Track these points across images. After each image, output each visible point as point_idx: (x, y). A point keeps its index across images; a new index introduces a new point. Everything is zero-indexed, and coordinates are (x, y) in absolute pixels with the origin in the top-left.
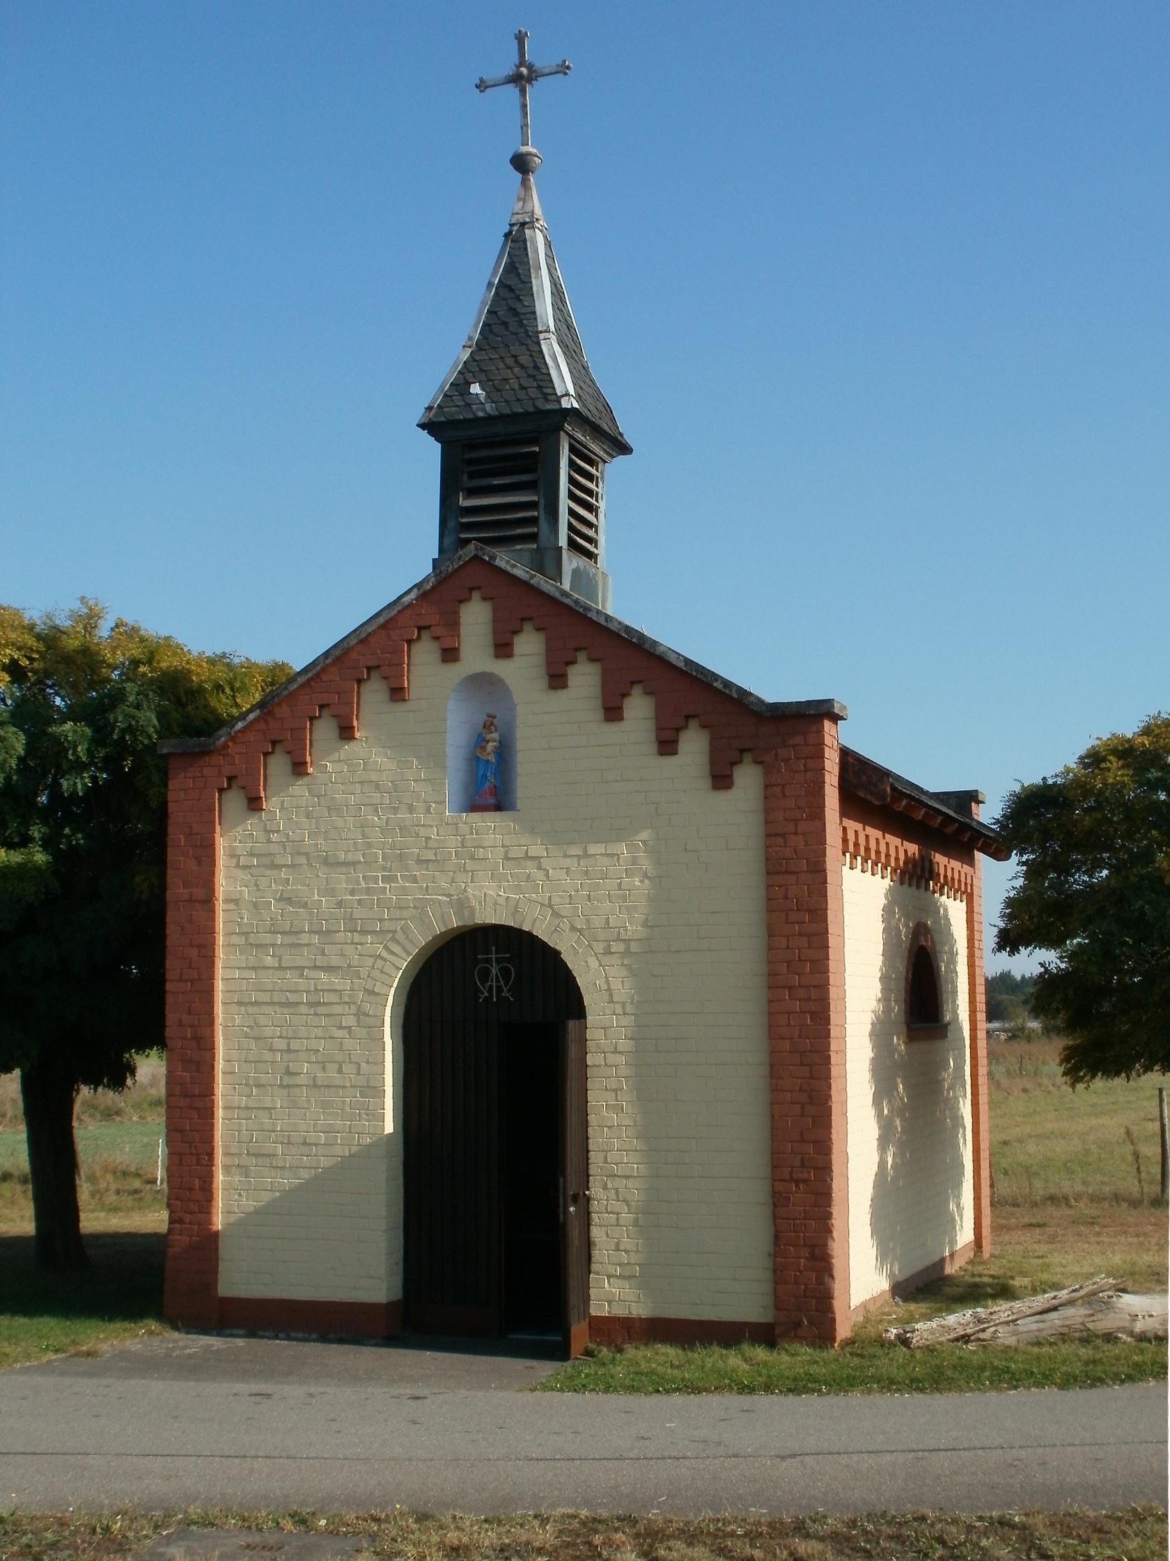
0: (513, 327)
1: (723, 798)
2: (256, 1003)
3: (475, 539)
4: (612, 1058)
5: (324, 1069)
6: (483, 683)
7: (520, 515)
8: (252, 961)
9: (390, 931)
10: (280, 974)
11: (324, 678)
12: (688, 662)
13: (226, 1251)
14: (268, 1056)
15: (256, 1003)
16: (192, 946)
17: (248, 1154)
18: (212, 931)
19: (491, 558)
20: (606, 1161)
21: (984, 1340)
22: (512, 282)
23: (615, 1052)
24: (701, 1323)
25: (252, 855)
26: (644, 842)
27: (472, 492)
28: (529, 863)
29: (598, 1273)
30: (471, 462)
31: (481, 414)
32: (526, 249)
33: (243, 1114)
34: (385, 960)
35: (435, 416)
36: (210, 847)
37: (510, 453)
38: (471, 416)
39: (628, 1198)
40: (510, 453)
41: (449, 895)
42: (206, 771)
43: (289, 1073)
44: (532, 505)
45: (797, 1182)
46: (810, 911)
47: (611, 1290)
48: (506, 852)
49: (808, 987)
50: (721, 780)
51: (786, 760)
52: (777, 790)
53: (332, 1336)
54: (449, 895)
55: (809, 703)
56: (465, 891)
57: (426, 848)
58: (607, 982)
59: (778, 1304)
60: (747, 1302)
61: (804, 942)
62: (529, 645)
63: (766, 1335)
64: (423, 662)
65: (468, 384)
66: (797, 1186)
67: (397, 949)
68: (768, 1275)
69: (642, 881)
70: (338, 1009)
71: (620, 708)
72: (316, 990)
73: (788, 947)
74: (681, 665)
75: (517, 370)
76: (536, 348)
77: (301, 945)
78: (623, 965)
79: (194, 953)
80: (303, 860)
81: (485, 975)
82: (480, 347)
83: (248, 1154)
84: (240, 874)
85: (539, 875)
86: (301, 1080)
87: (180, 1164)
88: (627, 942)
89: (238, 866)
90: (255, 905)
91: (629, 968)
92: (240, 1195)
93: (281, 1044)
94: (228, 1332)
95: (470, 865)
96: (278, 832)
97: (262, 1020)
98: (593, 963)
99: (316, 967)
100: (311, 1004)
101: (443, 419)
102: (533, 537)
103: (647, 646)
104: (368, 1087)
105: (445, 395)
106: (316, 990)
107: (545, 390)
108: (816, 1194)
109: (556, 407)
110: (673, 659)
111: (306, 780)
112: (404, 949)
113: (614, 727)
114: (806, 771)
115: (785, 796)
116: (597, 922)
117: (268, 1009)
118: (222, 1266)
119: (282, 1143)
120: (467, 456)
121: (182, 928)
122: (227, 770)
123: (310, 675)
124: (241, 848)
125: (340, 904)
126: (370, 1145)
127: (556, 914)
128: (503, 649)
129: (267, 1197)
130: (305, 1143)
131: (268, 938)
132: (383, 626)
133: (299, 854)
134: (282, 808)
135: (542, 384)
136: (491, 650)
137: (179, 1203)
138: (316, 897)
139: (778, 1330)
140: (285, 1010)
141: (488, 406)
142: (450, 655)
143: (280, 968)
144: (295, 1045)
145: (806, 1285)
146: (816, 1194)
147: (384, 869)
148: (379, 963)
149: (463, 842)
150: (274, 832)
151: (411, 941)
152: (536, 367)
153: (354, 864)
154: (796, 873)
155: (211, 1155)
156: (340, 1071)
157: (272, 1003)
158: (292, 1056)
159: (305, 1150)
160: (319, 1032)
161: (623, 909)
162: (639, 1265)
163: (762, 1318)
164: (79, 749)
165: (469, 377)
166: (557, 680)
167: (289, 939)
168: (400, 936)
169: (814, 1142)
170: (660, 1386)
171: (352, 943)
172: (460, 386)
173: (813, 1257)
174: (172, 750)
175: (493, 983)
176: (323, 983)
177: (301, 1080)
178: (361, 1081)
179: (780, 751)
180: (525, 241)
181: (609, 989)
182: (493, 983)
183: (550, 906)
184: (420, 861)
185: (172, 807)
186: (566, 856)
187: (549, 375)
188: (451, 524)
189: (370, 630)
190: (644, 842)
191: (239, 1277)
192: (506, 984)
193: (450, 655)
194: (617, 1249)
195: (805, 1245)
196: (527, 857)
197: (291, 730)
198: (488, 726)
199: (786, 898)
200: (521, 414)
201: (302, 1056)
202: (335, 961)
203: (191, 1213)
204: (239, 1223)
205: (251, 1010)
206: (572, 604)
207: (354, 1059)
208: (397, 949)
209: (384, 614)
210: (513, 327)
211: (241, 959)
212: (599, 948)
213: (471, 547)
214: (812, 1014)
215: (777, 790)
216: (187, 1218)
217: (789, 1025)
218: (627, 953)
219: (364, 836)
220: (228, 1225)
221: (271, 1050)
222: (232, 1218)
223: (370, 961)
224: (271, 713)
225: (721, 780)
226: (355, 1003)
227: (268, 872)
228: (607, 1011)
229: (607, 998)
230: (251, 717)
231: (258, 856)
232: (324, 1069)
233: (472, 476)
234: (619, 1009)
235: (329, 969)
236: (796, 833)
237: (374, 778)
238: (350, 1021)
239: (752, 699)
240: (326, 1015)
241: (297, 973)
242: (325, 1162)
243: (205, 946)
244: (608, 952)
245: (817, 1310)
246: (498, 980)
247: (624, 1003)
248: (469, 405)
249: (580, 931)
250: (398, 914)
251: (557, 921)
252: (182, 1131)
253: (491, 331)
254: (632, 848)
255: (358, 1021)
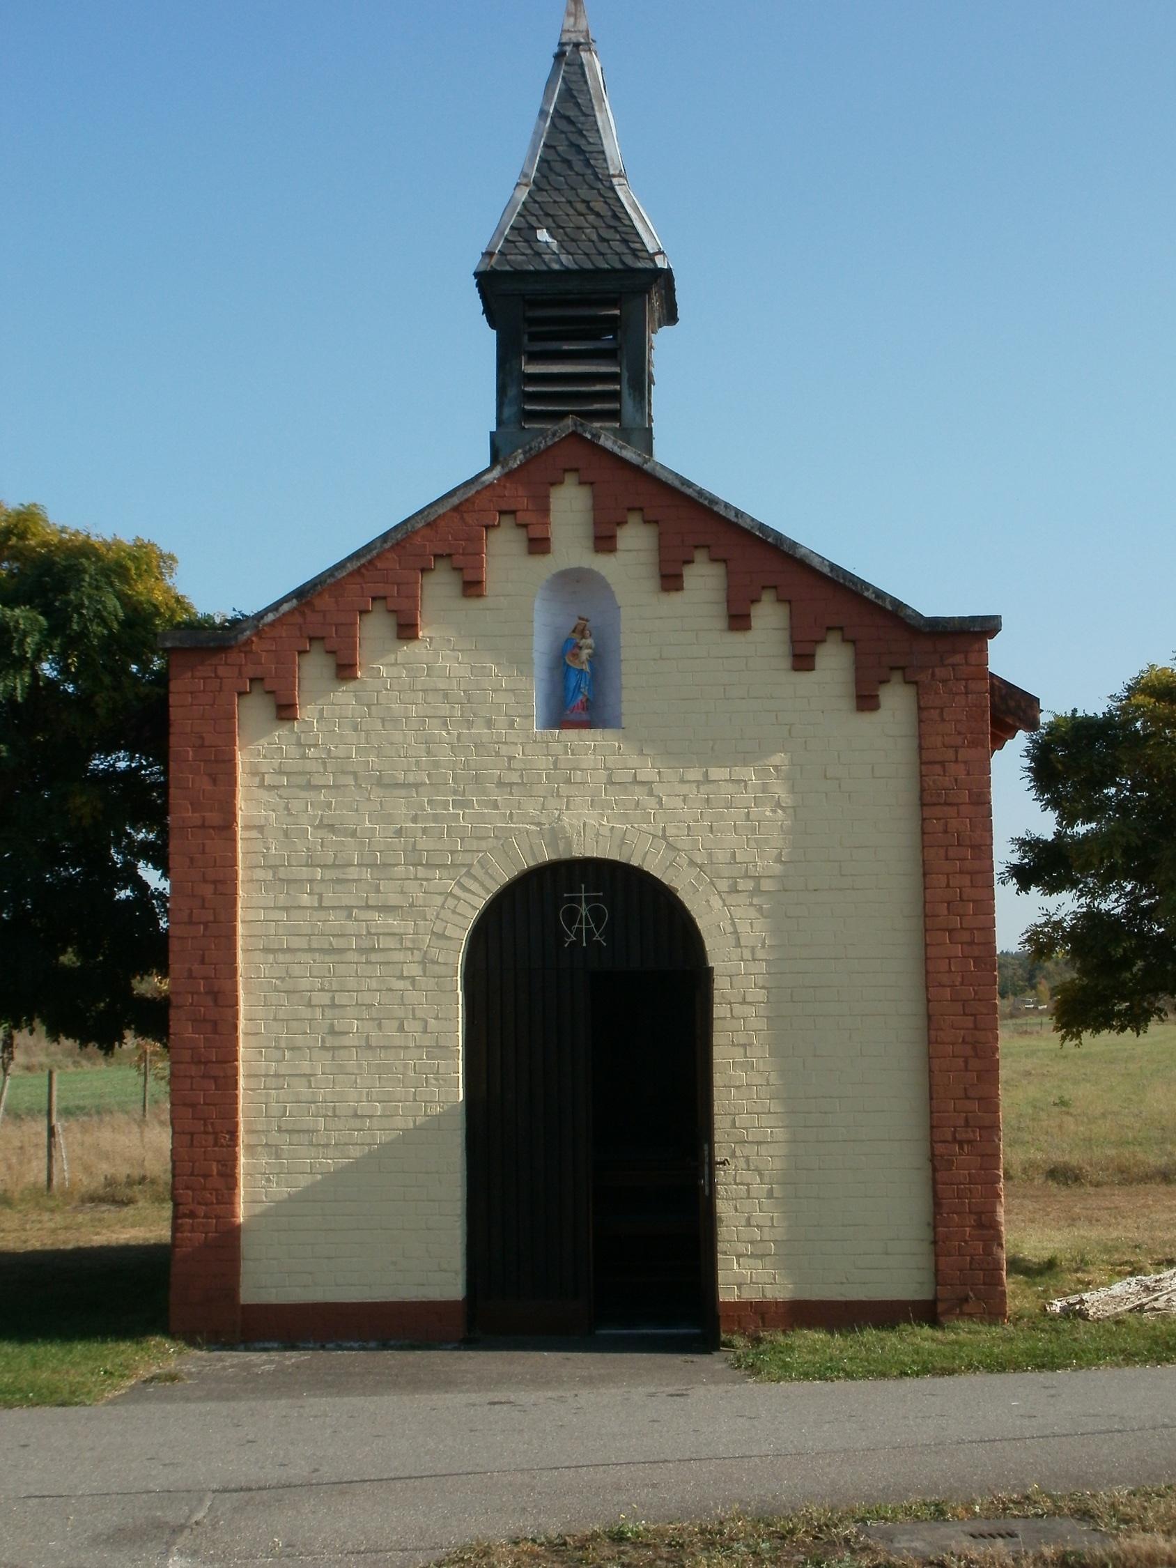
0: (578, 166)
1: (868, 720)
2: (289, 950)
3: (573, 412)
4: (738, 1010)
5: (380, 1027)
6: (573, 582)
7: (598, 388)
8: (282, 900)
9: (463, 865)
10: (322, 915)
11: (379, 565)
12: (833, 567)
13: (249, 1247)
14: (305, 1012)
15: (289, 950)
16: (205, 881)
17: (280, 1130)
18: (233, 863)
19: (593, 435)
20: (733, 1125)
21: (1159, 1310)
22: (572, 113)
23: (744, 1002)
24: (848, 1304)
25: (280, 772)
26: (776, 767)
27: (534, 357)
28: (637, 789)
29: (725, 1253)
30: (532, 321)
31: (556, 267)
32: (584, 75)
33: (272, 1082)
34: (459, 899)
35: (498, 263)
36: (232, 761)
37: (572, 315)
38: (544, 268)
39: (761, 1167)
40: (572, 315)
41: (539, 824)
42: (222, 671)
43: (333, 1032)
44: (614, 378)
45: (961, 1143)
46: (972, 847)
47: (746, 1269)
48: (610, 776)
49: (971, 929)
50: (866, 701)
51: (944, 681)
52: (935, 714)
53: (392, 1343)
54: (539, 824)
55: (973, 619)
56: (559, 819)
57: (509, 769)
58: (733, 924)
59: (938, 1276)
60: (899, 1274)
61: (966, 880)
62: (636, 540)
63: (928, 1313)
64: (502, 552)
65: (534, 229)
66: (961, 1148)
67: (474, 886)
68: (926, 1247)
69: (774, 811)
70: (398, 956)
71: (747, 617)
72: (369, 933)
73: (948, 886)
74: (826, 570)
75: (591, 218)
76: (610, 194)
77: (348, 880)
78: (751, 904)
79: (208, 890)
80: (350, 780)
81: (572, 915)
82: (538, 187)
83: (280, 1130)
84: (265, 795)
85: (652, 802)
86: (348, 1041)
87: (192, 1145)
88: (757, 879)
89: (261, 785)
90: (286, 834)
91: (760, 909)
92: (268, 1180)
93: (325, 999)
94: (257, 1345)
95: (564, 789)
96: (315, 746)
97: (296, 970)
98: (716, 902)
99: (368, 907)
100: (360, 950)
101: (508, 268)
102: (614, 415)
103: (785, 548)
104: (438, 1046)
105: (507, 240)
106: (369, 933)
107: (632, 245)
108: (982, 1156)
109: (649, 265)
110: (816, 563)
111: (352, 685)
112: (482, 885)
113: (738, 637)
114: (967, 693)
115: (943, 720)
116: (721, 856)
117: (306, 957)
118: (246, 1267)
119: (325, 1116)
120: (530, 314)
121: (192, 860)
122: (251, 670)
123: (363, 561)
124: (266, 765)
125: (399, 833)
126: (441, 1115)
127: (671, 847)
128: (604, 542)
129: (304, 1181)
130: (356, 1116)
131: (305, 873)
132: (456, 509)
133: (343, 772)
134: (321, 718)
135: (626, 237)
136: (590, 544)
137: (190, 1193)
138: (368, 824)
139: (941, 1307)
140: (327, 958)
141: (563, 258)
142: (539, 545)
143: (321, 907)
144: (341, 999)
145: (971, 1256)
146: (982, 1156)
147: (455, 792)
148: (451, 902)
149: (555, 763)
150: (310, 746)
151: (491, 877)
152: (615, 216)
153: (417, 786)
154: (957, 805)
155: (233, 1133)
156: (401, 1028)
157: (310, 950)
158: (337, 1011)
159: (357, 1123)
160: (374, 984)
161: (752, 843)
162: (775, 1242)
163: (925, 1294)
164: (29, 640)
165: (533, 220)
166: (670, 581)
167: (332, 874)
168: (477, 871)
169: (980, 1099)
170: (824, 1372)
171: (416, 879)
172: (523, 231)
173: (980, 1225)
174: (178, 644)
175: (583, 924)
176: (377, 926)
177: (348, 1041)
178: (428, 1040)
179: (937, 670)
180: (582, 65)
181: (735, 932)
182: (583, 924)
183: (664, 837)
184: (500, 784)
185: (175, 713)
186: (682, 781)
187: (634, 227)
188: (512, 392)
189: (441, 511)
190: (776, 767)
191: (265, 1280)
192: (598, 928)
193: (539, 545)
194: (749, 1225)
195: (970, 1212)
196: (635, 782)
197: (337, 625)
198: (580, 631)
199: (946, 832)
200: (607, 271)
201: (350, 1011)
202: (394, 900)
203: (206, 1204)
204: (264, 1215)
205: (281, 957)
206: (694, 495)
207: (419, 1014)
208: (474, 886)
209: (459, 493)
210: (578, 166)
211: (266, 898)
212: (723, 885)
213: (569, 421)
214: (976, 959)
215: (935, 714)
216: (201, 1210)
217: (950, 971)
218: (757, 891)
219: (428, 752)
220: (251, 1217)
221: (310, 1005)
222: (258, 1209)
223: (439, 900)
224: (309, 604)
225: (866, 701)
226: (419, 949)
227: (303, 794)
228: (734, 957)
229: (733, 942)
230: (286, 607)
231: (288, 774)
232: (380, 1027)
233: (534, 337)
234: (747, 954)
235: (385, 909)
236: (956, 761)
237: (441, 686)
238: (415, 970)
239: (910, 612)
240: (381, 963)
241: (345, 913)
242: (381, 1137)
243: (223, 882)
244: (734, 890)
245: (984, 1284)
246: (588, 923)
247: (753, 948)
248: (538, 254)
249: (701, 867)
250: (475, 845)
251: (672, 855)
252: (193, 1106)
253: (551, 169)
254: (762, 773)
255: (424, 971)
